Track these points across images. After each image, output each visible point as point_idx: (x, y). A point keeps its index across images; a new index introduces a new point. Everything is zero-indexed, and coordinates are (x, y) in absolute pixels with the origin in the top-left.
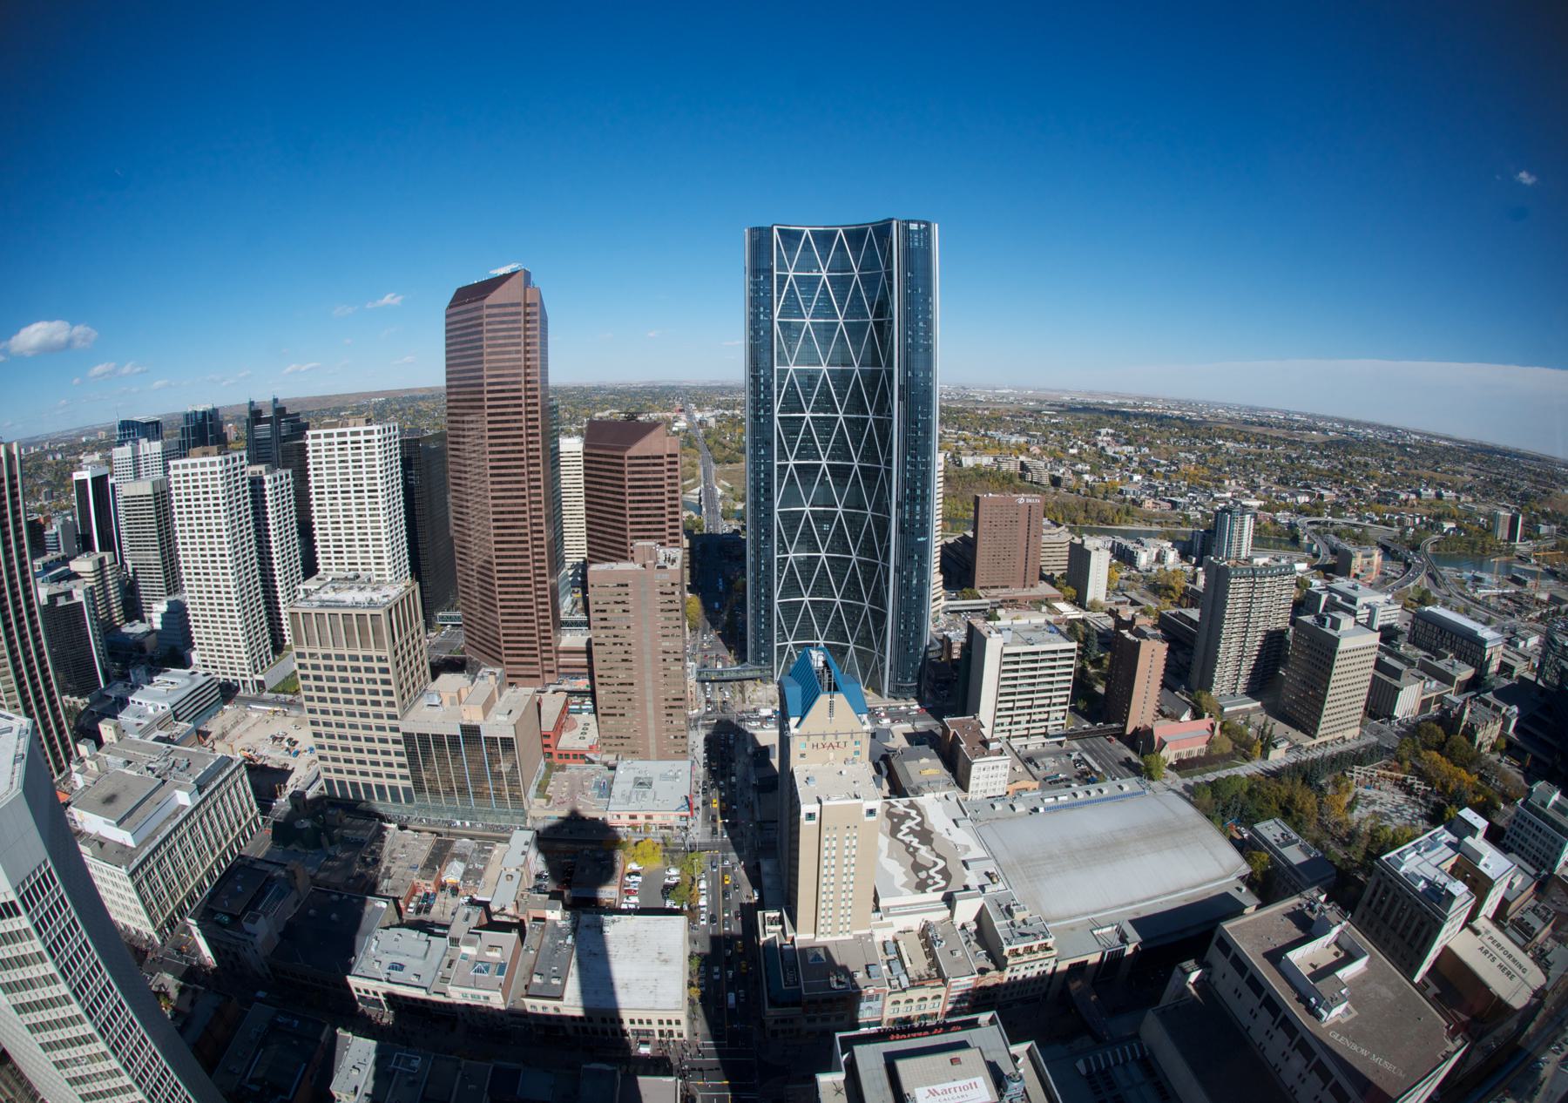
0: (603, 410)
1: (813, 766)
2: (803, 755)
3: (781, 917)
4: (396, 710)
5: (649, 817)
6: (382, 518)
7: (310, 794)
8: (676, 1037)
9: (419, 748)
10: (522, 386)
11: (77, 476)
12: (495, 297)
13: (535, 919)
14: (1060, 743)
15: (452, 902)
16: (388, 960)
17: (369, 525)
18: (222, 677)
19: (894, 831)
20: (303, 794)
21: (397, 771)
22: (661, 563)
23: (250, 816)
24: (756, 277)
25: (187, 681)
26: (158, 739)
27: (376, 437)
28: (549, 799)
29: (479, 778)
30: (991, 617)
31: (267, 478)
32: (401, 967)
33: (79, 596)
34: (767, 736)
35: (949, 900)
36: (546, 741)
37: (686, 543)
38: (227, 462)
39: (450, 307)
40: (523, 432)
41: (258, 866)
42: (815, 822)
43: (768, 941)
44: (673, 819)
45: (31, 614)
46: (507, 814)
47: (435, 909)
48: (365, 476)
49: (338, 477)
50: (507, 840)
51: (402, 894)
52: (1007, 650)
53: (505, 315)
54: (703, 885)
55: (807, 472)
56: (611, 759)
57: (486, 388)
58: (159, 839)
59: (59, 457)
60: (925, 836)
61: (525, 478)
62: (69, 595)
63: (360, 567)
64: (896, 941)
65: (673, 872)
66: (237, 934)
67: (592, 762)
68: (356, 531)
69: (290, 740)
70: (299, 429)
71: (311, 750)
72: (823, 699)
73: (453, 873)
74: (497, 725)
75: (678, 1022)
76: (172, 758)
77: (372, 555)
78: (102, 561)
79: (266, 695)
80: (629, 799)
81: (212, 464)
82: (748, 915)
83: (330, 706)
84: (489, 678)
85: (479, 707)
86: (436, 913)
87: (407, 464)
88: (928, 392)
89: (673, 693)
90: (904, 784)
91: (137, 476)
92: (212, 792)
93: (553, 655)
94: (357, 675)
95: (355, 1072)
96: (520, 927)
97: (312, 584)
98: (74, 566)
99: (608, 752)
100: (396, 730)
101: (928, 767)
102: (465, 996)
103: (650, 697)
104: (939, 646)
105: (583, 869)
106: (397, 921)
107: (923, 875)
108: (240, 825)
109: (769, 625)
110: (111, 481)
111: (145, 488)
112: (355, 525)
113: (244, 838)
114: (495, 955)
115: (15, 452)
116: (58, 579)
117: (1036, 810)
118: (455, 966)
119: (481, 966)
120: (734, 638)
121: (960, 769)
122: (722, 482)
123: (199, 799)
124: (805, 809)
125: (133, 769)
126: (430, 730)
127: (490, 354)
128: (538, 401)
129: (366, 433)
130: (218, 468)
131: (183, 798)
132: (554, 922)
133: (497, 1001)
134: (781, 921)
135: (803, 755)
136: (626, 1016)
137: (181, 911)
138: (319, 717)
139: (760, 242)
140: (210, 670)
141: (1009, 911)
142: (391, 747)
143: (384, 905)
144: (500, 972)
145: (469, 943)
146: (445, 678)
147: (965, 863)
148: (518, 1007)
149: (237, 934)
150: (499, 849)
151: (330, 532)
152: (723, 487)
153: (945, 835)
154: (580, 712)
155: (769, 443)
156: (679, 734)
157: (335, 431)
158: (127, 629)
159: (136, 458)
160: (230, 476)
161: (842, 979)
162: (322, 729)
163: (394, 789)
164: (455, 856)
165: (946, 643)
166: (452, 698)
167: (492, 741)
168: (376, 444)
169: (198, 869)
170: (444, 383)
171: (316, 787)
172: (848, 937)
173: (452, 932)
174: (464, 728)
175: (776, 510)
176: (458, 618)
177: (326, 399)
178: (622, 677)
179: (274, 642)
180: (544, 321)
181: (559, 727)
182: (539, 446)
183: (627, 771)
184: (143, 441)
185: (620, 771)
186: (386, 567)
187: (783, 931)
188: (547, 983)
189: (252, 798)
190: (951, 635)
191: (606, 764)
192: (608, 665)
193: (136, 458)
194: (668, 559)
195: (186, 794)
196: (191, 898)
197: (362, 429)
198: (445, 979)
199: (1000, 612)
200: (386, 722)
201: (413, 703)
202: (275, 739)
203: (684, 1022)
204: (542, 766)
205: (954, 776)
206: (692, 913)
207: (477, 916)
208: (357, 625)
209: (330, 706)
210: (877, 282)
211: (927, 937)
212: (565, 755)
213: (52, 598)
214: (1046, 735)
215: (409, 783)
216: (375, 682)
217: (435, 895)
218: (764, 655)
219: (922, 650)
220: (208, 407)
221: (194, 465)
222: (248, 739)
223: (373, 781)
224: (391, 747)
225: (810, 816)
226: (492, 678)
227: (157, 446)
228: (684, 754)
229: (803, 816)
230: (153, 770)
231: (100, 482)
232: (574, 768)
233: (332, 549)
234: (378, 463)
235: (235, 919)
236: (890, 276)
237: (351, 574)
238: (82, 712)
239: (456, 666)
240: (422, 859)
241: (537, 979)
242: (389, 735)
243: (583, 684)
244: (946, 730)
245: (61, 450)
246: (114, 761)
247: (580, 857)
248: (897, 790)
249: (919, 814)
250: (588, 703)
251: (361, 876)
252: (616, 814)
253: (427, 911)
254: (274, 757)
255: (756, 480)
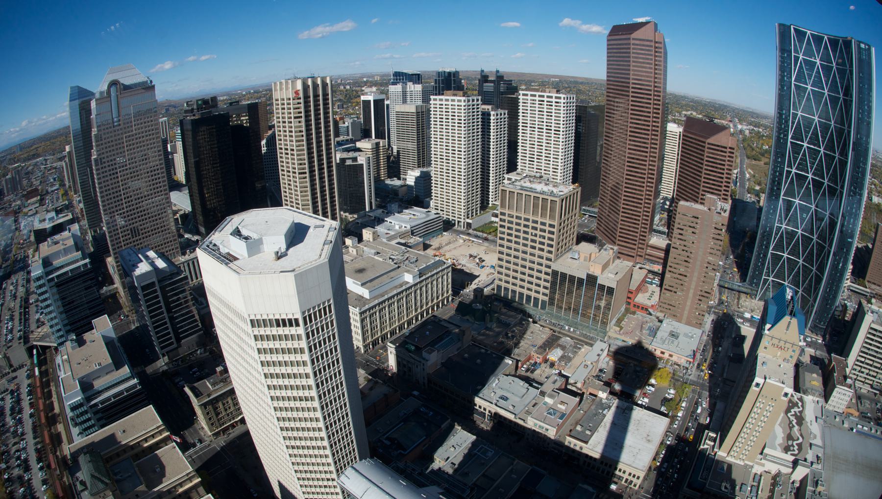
0: (687, 111)
1: (768, 356)
2: (765, 348)
3: (716, 438)
4: (552, 256)
5: (671, 356)
6: (560, 147)
7: (487, 291)
8: (632, 486)
9: (559, 280)
10: (652, 88)
11: (363, 98)
12: (637, 34)
13: (591, 394)
14: (875, 394)
15: (548, 371)
16: (500, 393)
17: (552, 149)
18: (445, 217)
19: (788, 411)
20: (482, 290)
21: (541, 290)
22: (718, 210)
23: (445, 295)
24: (783, 54)
25: (424, 215)
26: (399, 243)
27: (562, 101)
28: (621, 328)
29: (587, 306)
30: (869, 302)
31: (492, 113)
32: (504, 398)
33: (362, 160)
34: (748, 331)
35: (795, 463)
36: (630, 295)
37: (730, 201)
38: (469, 101)
39: (610, 35)
40: (651, 115)
41: (442, 323)
42: (758, 389)
43: (703, 449)
44: (683, 361)
45: (330, 167)
46: (596, 330)
47: (538, 372)
48: (553, 121)
49: (537, 119)
50: (591, 345)
51: (522, 359)
52: (873, 326)
53: (643, 45)
54: (684, 405)
55: (801, 179)
56: (661, 315)
57: (631, 86)
58: (386, 297)
59: (348, 87)
60: (800, 419)
61: (649, 142)
62: (355, 159)
63: (543, 171)
64: (761, 476)
65: (672, 391)
66: (417, 358)
67: (650, 314)
68: (544, 151)
69: (480, 259)
70: (515, 90)
71: (493, 267)
72: (787, 318)
73: (555, 355)
74: (607, 279)
75: (638, 478)
76: (408, 255)
77: (551, 166)
78: (378, 144)
79: (471, 231)
80: (664, 342)
81: (459, 101)
82: (701, 429)
83: (513, 245)
84: (609, 251)
85: (600, 267)
86: (537, 375)
87: (578, 119)
88: (867, 150)
89: (706, 288)
90: (801, 385)
91: (404, 101)
92: (428, 278)
93: (644, 247)
94: (534, 232)
95: (452, 449)
96: (581, 395)
97: (513, 176)
98: (359, 145)
99: (661, 311)
100: (549, 267)
101: (814, 380)
102: (535, 425)
103: (693, 286)
104: (840, 308)
105: (626, 374)
106: (513, 373)
107: (790, 443)
108: (440, 301)
109: (763, 264)
110: (386, 102)
111: (411, 108)
112: (544, 148)
113: (438, 306)
114: (562, 407)
115: (328, 81)
116: (348, 150)
117: (852, 429)
118: (537, 407)
119: (552, 411)
120: (743, 266)
121: (828, 389)
122: (750, 170)
123: (418, 280)
124: (758, 380)
125: (381, 257)
126: (569, 272)
127: (634, 66)
128: (661, 98)
129: (556, 98)
130: (463, 104)
131: (409, 278)
132: (601, 399)
133: (552, 433)
134: (714, 440)
135: (765, 348)
136: (620, 466)
137: (384, 338)
138: (505, 250)
139: (784, 31)
140: (439, 211)
141: (816, 484)
142: (543, 276)
143: (510, 362)
144: (561, 418)
145: (551, 396)
146: (584, 245)
147: (811, 445)
148: (561, 439)
149: (417, 358)
150: (585, 349)
151: (528, 149)
152: (749, 173)
153: (809, 424)
154: (651, 283)
155: (783, 156)
156: (702, 313)
157: (537, 94)
158: (388, 182)
159: (404, 93)
160: (470, 109)
161: (728, 486)
162: (505, 257)
163: (536, 300)
164: (559, 345)
165: (845, 307)
166: (585, 257)
167: (602, 287)
168: (562, 105)
169: (404, 318)
170: (605, 78)
171: (489, 288)
172: (742, 463)
173: (543, 388)
174: (588, 276)
175: (781, 197)
176: (594, 213)
177: (523, 74)
178: (682, 270)
179: (482, 203)
180: (666, 53)
181: (639, 289)
182: (659, 125)
183: (668, 325)
184: (410, 84)
185: (664, 324)
186: (559, 174)
187: (714, 446)
188: (583, 432)
189: (450, 286)
190: (848, 304)
191: (658, 318)
192: (676, 261)
193: (404, 93)
194: (722, 209)
195: (411, 276)
196: (393, 333)
197: (554, 95)
198: (528, 413)
199: (873, 300)
200: (544, 262)
201: (562, 254)
202: (471, 256)
203: (641, 479)
204: (623, 309)
205: (825, 391)
206: (673, 418)
207: (560, 382)
208: (541, 204)
209: (513, 245)
210: (844, 73)
211: (776, 479)
212: (637, 306)
213: (343, 160)
214: (872, 387)
215: (546, 299)
216: (544, 238)
217: (540, 364)
218: (755, 282)
219: (834, 308)
220: (453, 70)
221: (447, 100)
222: (456, 253)
223: (525, 292)
224: (543, 276)
225: (757, 385)
226: (611, 251)
227: (419, 87)
228: (700, 325)
229: (754, 383)
230: (393, 260)
231: (379, 103)
232: (640, 315)
233: (528, 159)
234: (562, 115)
235: (418, 349)
236: (851, 72)
237: (538, 175)
238: (350, 222)
239: (590, 239)
240: (540, 342)
241: (579, 428)
242: (544, 269)
243: (658, 268)
244: (830, 361)
245: (349, 84)
246: (368, 251)
247: (633, 368)
248: (797, 388)
249: (802, 406)
250: (657, 280)
251: (502, 343)
252: (656, 347)
253: (532, 372)
254: (470, 267)
255: (774, 175)
